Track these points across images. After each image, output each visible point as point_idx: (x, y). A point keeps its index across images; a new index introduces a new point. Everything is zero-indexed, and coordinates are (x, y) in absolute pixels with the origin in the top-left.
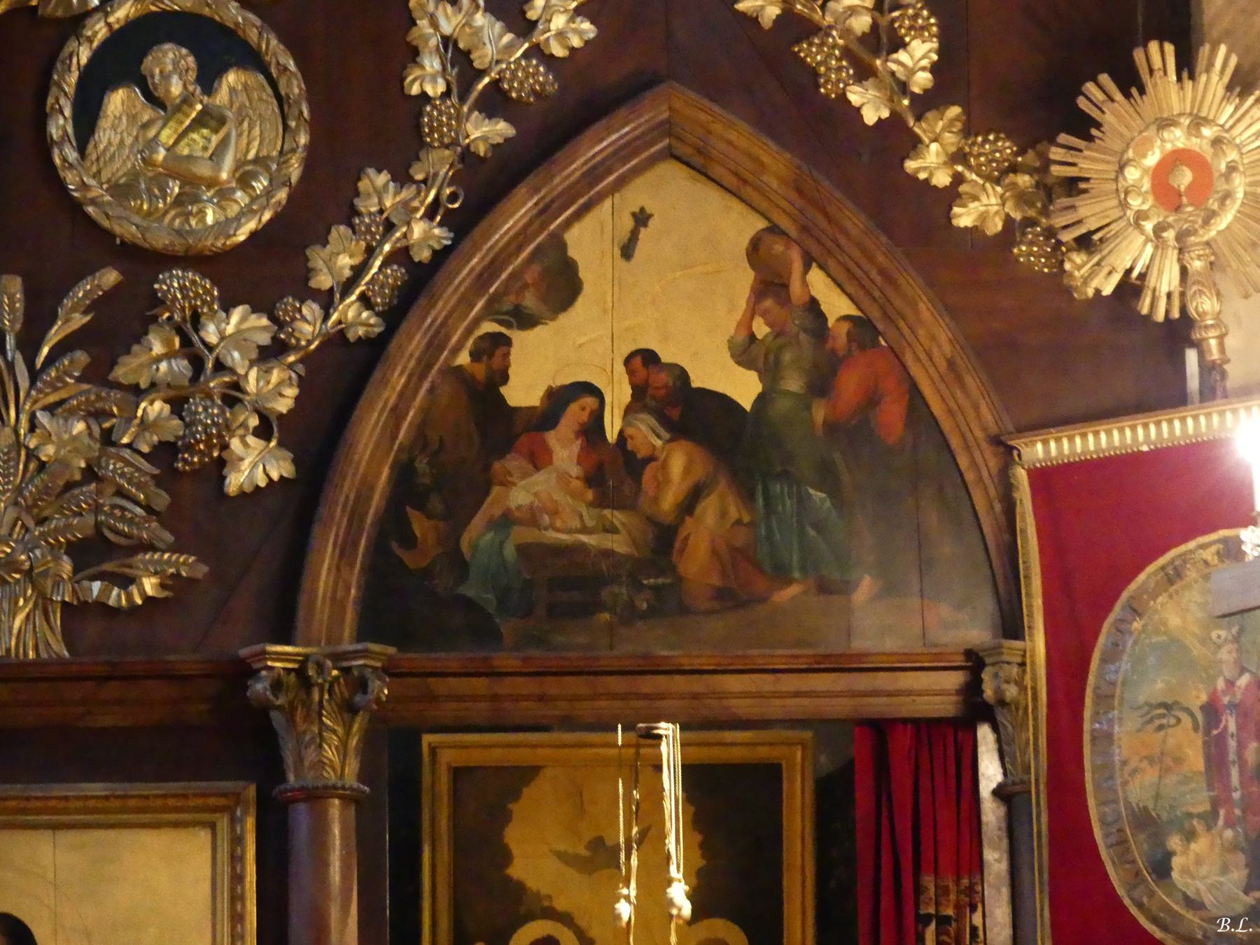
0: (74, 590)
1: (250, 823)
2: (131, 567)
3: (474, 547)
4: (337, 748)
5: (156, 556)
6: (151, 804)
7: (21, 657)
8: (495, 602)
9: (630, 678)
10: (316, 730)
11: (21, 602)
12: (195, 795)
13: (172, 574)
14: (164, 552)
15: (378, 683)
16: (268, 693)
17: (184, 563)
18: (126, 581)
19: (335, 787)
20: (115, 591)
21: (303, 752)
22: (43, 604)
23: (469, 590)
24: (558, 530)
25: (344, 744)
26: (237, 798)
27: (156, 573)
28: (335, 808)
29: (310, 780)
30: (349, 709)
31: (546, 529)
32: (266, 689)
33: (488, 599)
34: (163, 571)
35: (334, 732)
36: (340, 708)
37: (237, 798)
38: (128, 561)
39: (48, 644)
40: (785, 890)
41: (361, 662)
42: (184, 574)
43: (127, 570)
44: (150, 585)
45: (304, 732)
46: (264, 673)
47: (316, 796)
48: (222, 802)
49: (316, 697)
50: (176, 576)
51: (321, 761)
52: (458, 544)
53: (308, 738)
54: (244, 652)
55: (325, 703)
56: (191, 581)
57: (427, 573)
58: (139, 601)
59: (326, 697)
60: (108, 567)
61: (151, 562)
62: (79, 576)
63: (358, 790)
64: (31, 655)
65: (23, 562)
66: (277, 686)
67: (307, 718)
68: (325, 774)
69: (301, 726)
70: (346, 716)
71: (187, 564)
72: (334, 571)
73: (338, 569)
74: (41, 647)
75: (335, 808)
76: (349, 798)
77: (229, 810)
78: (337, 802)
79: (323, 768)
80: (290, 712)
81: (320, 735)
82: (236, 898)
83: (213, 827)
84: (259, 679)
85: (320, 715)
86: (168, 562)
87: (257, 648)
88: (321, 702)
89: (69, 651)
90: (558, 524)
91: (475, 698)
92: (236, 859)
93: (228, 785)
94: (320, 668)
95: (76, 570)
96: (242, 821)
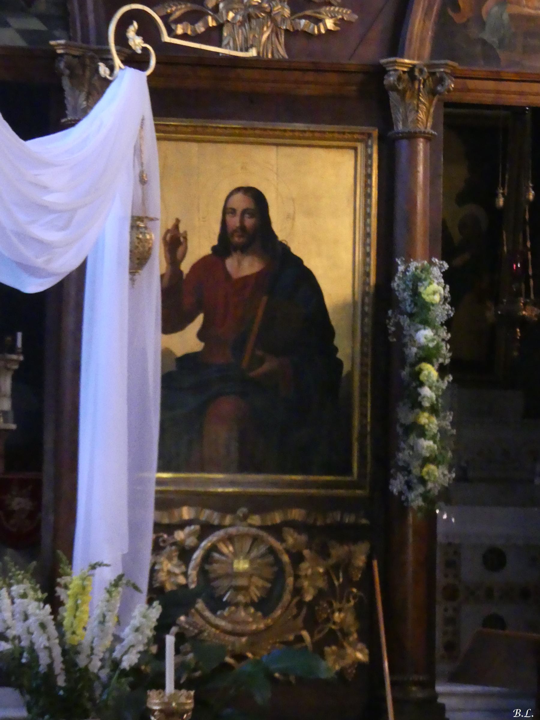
0: (291, 24)
1: (375, 148)
2: (320, 13)
3: (488, 13)
4: (425, 113)
5: (332, 8)
6: (326, 136)
7: (265, 56)
8: (497, 42)
9: (518, 83)
10: (415, 102)
11: (265, 29)
12: (349, 133)
13: (340, 19)
14: (336, 6)
15: (449, 81)
16: (396, 83)
17: (346, 13)
18: (318, 21)
19: (420, 132)
20: (312, 25)
21: (408, 114)
22: (276, 32)
23: (486, 36)
24: (529, 7)
25: (428, 111)
26: (370, 135)
27: (332, 17)
28: (421, 145)
29: (411, 127)
30: (433, 93)
31: (524, 7)
32: (394, 81)
33: (493, 40)
34: (335, 17)
35: (424, 104)
36: (428, 93)
37: (370, 135)
38: (318, 10)
39: (278, 51)
40: (284, 124)
41: (442, 70)
42: (345, 19)
43: (318, 15)
44: (330, 24)
45: (410, 104)
46: (391, 73)
47: (412, 136)
48: (359, 137)
49: (417, 87)
50: (342, 19)
51: (417, 119)
52: (481, 12)
53: (411, 107)
54: (383, 61)
55: (421, 90)
56: (350, 23)
57: (465, 25)
58: (323, 31)
59: (422, 86)
60: (308, 12)
61: (330, 12)
62: (293, 18)
63: (432, 134)
64: (270, 56)
65: (266, 8)
66: (399, 79)
67: (412, 97)
68: (419, 126)
69: (408, 100)
70: (431, 96)
71: (347, 14)
72: (422, 22)
73: (424, 21)
74: (275, 51)
75: (421, 145)
76: (428, 138)
77: (364, 142)
78: (422, 140)
79: (418, 123)
80: (402, 94)
81: (418, 107)
82: (367, 186)
83: (355, 149)
84: (390, 76)
85: (419, 95)
86: (338, 12)
87: (392, 59)
88: (419, 88)
89: (288, 55)
90: (530, 4)
91: (488, 91)
92: (368, 166)
93: (364, 129)
94: (421, 71)
95: (292, 13)
96: (371, 147)
